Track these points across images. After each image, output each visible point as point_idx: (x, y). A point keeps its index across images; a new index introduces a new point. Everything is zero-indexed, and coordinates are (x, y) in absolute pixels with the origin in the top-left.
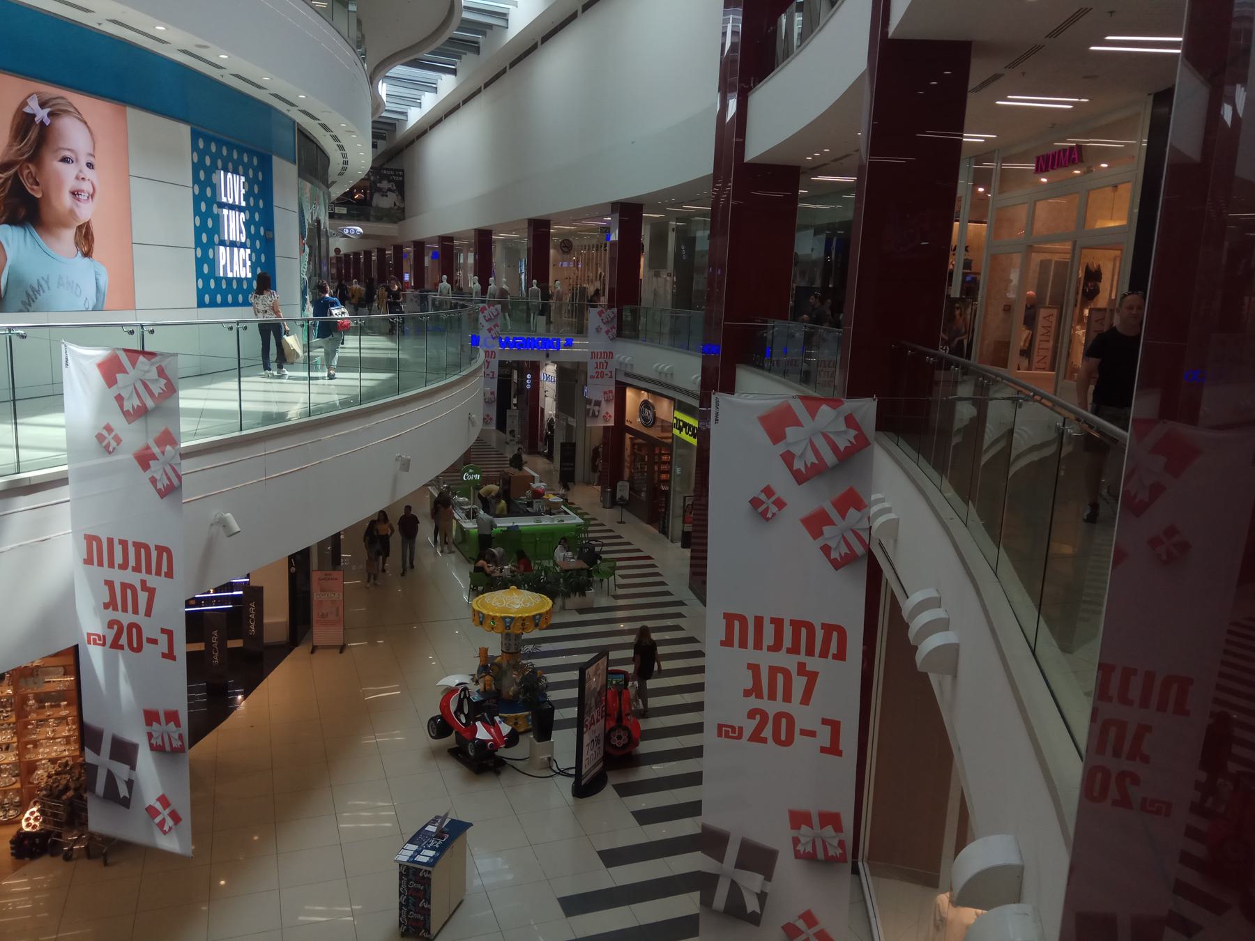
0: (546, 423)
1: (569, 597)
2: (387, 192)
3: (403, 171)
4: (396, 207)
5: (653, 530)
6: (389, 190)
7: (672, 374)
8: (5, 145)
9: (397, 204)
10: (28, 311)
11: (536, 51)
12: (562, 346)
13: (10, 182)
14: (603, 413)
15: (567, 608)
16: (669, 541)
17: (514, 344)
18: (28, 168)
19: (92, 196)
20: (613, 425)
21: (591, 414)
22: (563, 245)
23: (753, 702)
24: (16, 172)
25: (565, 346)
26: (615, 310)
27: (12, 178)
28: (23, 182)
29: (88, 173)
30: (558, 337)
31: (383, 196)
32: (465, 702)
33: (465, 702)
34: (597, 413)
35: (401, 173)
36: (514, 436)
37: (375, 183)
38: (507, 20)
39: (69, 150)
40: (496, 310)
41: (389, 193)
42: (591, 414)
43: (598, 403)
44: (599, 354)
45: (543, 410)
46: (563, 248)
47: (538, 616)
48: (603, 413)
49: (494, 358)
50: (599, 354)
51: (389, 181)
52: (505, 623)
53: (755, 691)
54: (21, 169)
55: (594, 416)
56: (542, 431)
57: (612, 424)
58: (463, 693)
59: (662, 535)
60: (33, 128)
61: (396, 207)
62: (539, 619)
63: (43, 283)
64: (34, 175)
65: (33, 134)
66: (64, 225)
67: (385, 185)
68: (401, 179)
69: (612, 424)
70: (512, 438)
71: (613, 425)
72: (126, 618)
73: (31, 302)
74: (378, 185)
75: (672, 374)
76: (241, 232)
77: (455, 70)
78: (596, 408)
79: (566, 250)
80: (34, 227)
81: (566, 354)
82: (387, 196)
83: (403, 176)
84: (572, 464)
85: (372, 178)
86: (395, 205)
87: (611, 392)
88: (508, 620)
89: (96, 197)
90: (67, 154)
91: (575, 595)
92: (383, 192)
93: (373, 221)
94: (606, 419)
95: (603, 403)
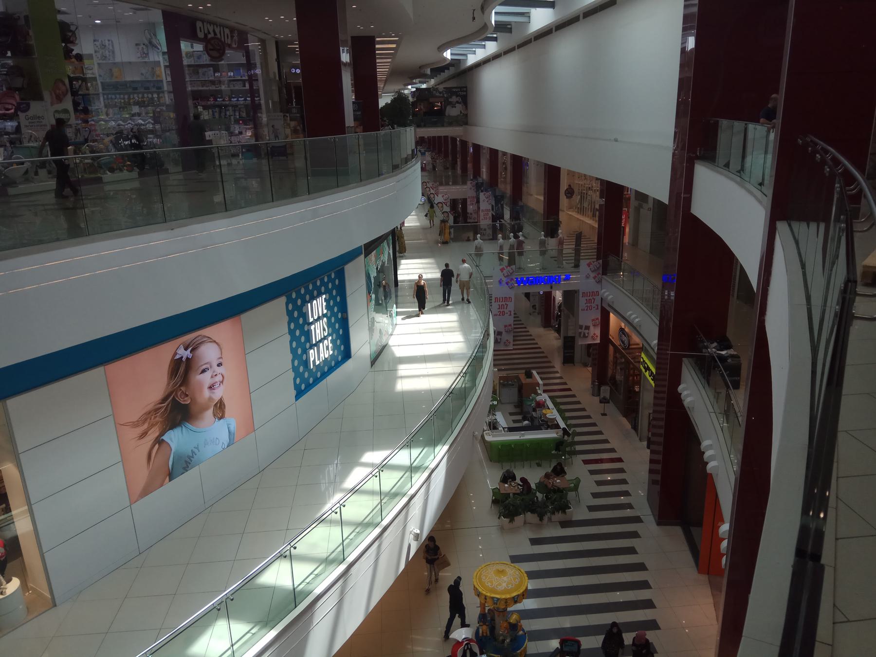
0: (557, 307)
1: (554, 514)
2: (455, 104)
3: (466, 87)
4: (462, 114)
5: (626, 424)
6: (457, 102)
7: (640, 326)
8: (165, 385)
9: (463, 112)
10: (187, 471)
11: (549, 36)
12: (562, 280)
13: (170, 405)
14: (592, 334)
15: (553, 521)
16: (638, 439)
17: (525, 283)
18: (181, 390)
19: (222, 382)
20: (599, 342)
21: (582, 336)
22: (567, 192)
23: (499, 310)
24: (174, 397)
25: (565, 280)
26: (601, 261)
27: (171, 402)
28: (178, 400)
29: (219, 370)
30: (559, 275)
31: (453, 107)
32: (468, 651)
33: (468, 651)
34: (587, 335)
35: (465, 89)
36: (535, 309)
37: (447, 99)
38: (530, 17)
39: (206, 364)
40: (512, 269)
41: (457, 105)
42: (582, 336)
43: (587, 328)
44: (501, 299)
45: (554, 298)
46: (567, 195)
47: (516, 597)
48: (592, 334)
49: (511, 301)
50: (501, 299)
51: (457, 96)
52: (494, 600)
53: (499, 308)
54: (176, 394)
55: (585, 337)
56: (554, 312)
57: (598, 341)
58: (466, 646)
59: (633, 431)
60: (182, 364)
61: (462, 114)
62: (517, 598)
63: (196, 451)
64: (184, 392)
65: (182, 369)
66: (206, 409)
67: (454, 99)
68: (465, 93)
69: (598, 341)
70: (534, 311)
71: (599, 342)
72: (502, 310)
73: (188, 465)
74: (450, 100)
75: (640, 326)
76: (324, 330)
77: (496, 37)
78: (587, 331)
79: (569, 195)
80: (189, 423)
81: (565, 285)
82: (455, 107)
83: (466, 91)
84: (572, 351)
85: (445, 96)
86: (461, 113)
87: (597, 319)
88: (495, 599)
89: (224, 382)
90: (204, 367)
91: (559, 512)
92: (453, 104)
93: (447, 126)
94: (593, 338)
95: (592, 328)
